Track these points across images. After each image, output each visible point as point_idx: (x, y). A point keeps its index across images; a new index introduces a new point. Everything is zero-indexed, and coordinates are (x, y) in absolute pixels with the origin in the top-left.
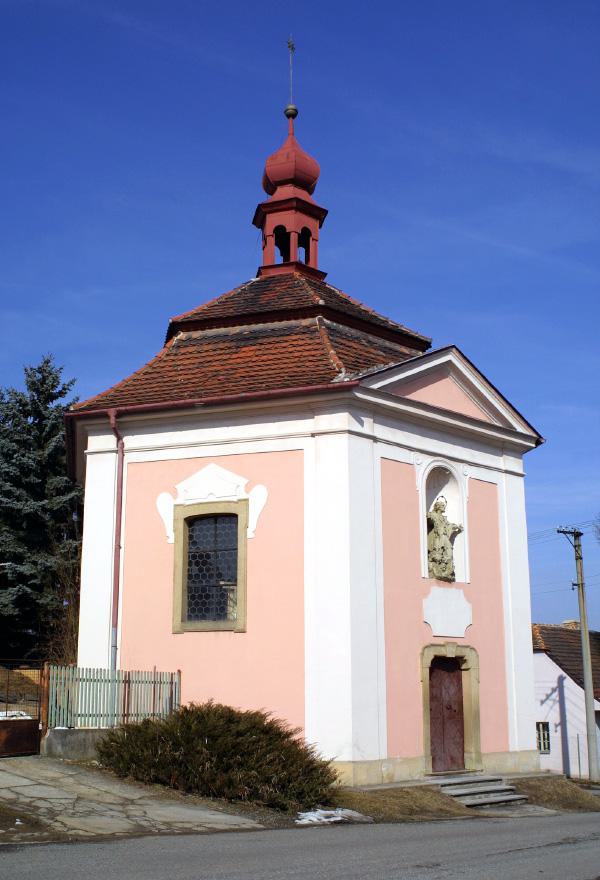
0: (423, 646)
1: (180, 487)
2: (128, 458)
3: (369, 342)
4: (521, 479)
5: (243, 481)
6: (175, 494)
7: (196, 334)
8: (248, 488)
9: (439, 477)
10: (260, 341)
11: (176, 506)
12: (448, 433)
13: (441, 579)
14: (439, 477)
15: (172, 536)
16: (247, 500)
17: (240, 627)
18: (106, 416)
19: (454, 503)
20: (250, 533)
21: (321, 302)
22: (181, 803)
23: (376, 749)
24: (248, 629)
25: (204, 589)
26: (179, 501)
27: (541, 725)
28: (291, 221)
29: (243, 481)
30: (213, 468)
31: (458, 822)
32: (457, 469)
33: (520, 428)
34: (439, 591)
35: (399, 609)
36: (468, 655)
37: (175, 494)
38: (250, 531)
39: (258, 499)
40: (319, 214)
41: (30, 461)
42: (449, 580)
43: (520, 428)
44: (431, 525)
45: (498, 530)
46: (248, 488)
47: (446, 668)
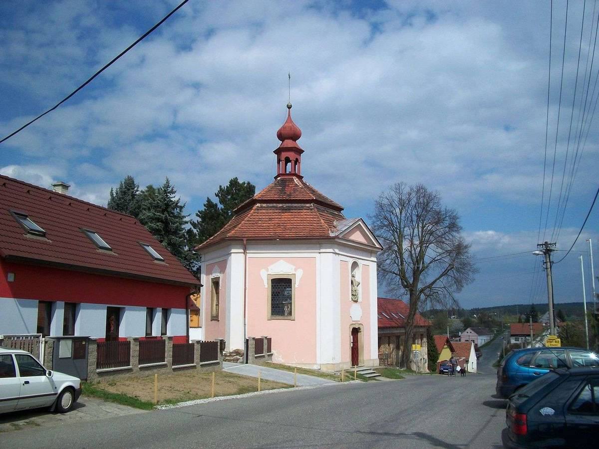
0: (350, 324)
1: (269, 268)
2: (248, 255)
3: (327, 211)
4: (376, 263)
5: (294, 267)
6: (268, 270)
7: (264, 205)
8: (296, 270)
9: (355, 265)
10: (291, 211)
12: (357, 249)
13: (354, 301)
14: (355, 265)
15: (267, 286)
17: (293, 318)
18: (242, 240)
19: (358, 272)
20: (296, 286)
21: (315, 198)
23: (338, 360)
24: (296, 319)
25: (277, 304)
28: (292, 155)
29: (294, 267)
30: (282, 261)
32: (359, 262)
33: (377, 246)
34: (355, 305)
35: (345, 311)
36: (361, 327)
38: (296, 284)
40: (300, 151)
41: (414, 300)
42: (356, 301)
43: (377, 246)
44: (352, 282)
46: (296, 270)
47: (355, 332)
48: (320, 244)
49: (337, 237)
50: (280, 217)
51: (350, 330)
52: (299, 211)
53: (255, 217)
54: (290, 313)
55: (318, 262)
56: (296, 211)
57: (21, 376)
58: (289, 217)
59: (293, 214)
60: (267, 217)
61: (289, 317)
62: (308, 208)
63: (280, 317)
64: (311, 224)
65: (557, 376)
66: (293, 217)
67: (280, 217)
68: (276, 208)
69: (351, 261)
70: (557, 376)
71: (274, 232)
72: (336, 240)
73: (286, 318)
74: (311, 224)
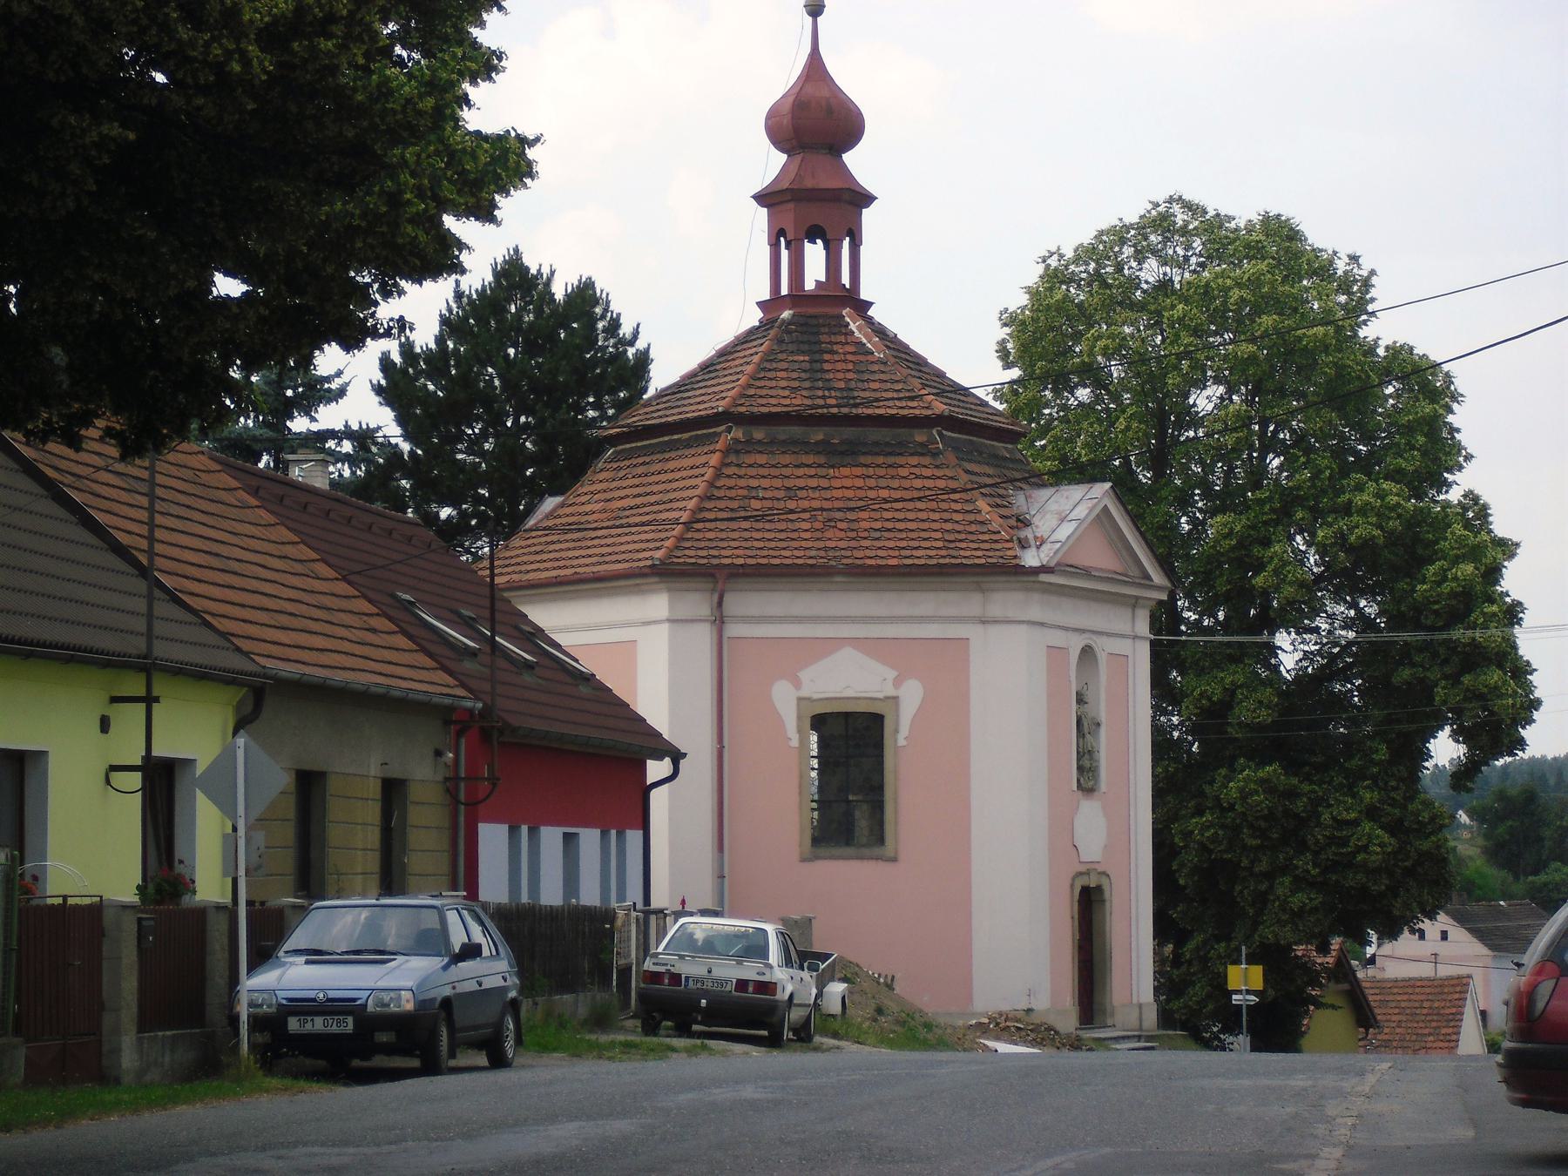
1: (805, 675)
2: (733, 630)
5: (891, 674)
6: (797, 684)
7: (759, 434)
8: (898, 682)
10: (862, 459)
11: (800, 699)
16: (896, 698)
17: (891, 854)
20: (901, 742)
22: (1069, 484)
26: (805, 693)
27: (691, 979)
29: (891, 674)
30: (848, 654)
31: (134, 652)
36: (1104, 882)
37: (797, 684)
38: (901, 735)
39: (911, 696)
45: (971, 912)
46: (898, 682)
48: (983, 591)
49: (1044, 569)
50: (824, 483)
51: (1072, 896)
52: (891, 460)
53: (731, 483)
54: (880, 840)
55: (975, 646)
56: (880, 460)
57: (1253, 1050)
58: (859, 482)
59: (871, 471)
60: (778, 483)
61: (877, 851)
62: (924, 450)
63: (850, 851)
64: (946, 516)
65: (650, 780)
66: (872, 483)
67: (824, 483)
68: (803, 446)
69: (1076, 644)
70: (650, 780)
71: (821, 544)
72: (1043, 577)
73: (866, 851)
74: (946, 516)
